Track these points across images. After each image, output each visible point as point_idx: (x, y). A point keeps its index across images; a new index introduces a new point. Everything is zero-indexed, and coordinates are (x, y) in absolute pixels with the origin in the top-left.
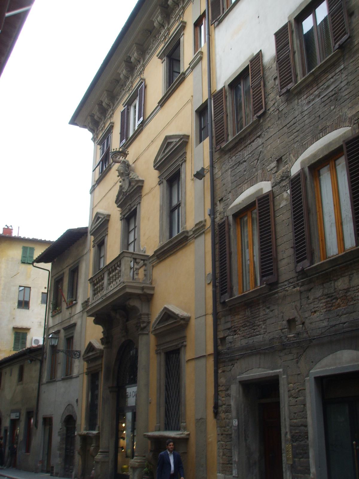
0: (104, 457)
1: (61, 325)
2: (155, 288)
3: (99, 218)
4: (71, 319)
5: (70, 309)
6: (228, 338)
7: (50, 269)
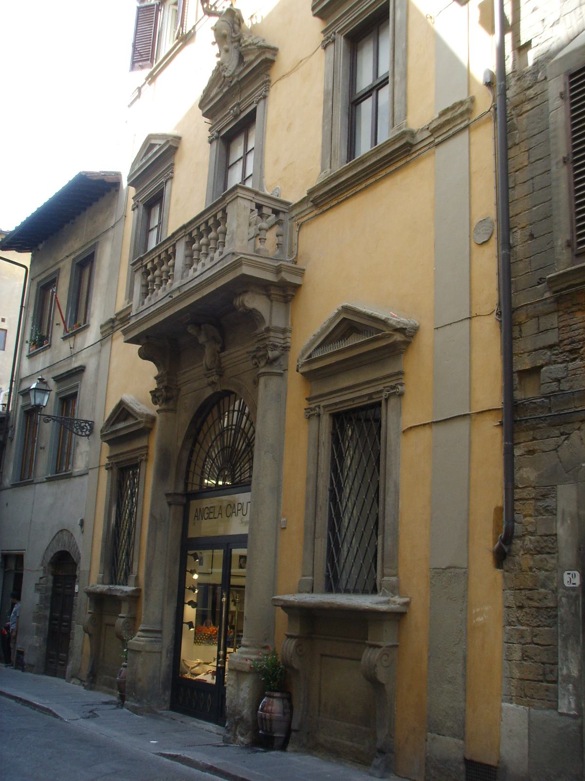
0: (151, 641)
1: (49, 372)
2: (306, 272)
3: (152, 146)
4: (74, 359)
5: (72, 339)
6: (546, 371)
7: (28, 264)
